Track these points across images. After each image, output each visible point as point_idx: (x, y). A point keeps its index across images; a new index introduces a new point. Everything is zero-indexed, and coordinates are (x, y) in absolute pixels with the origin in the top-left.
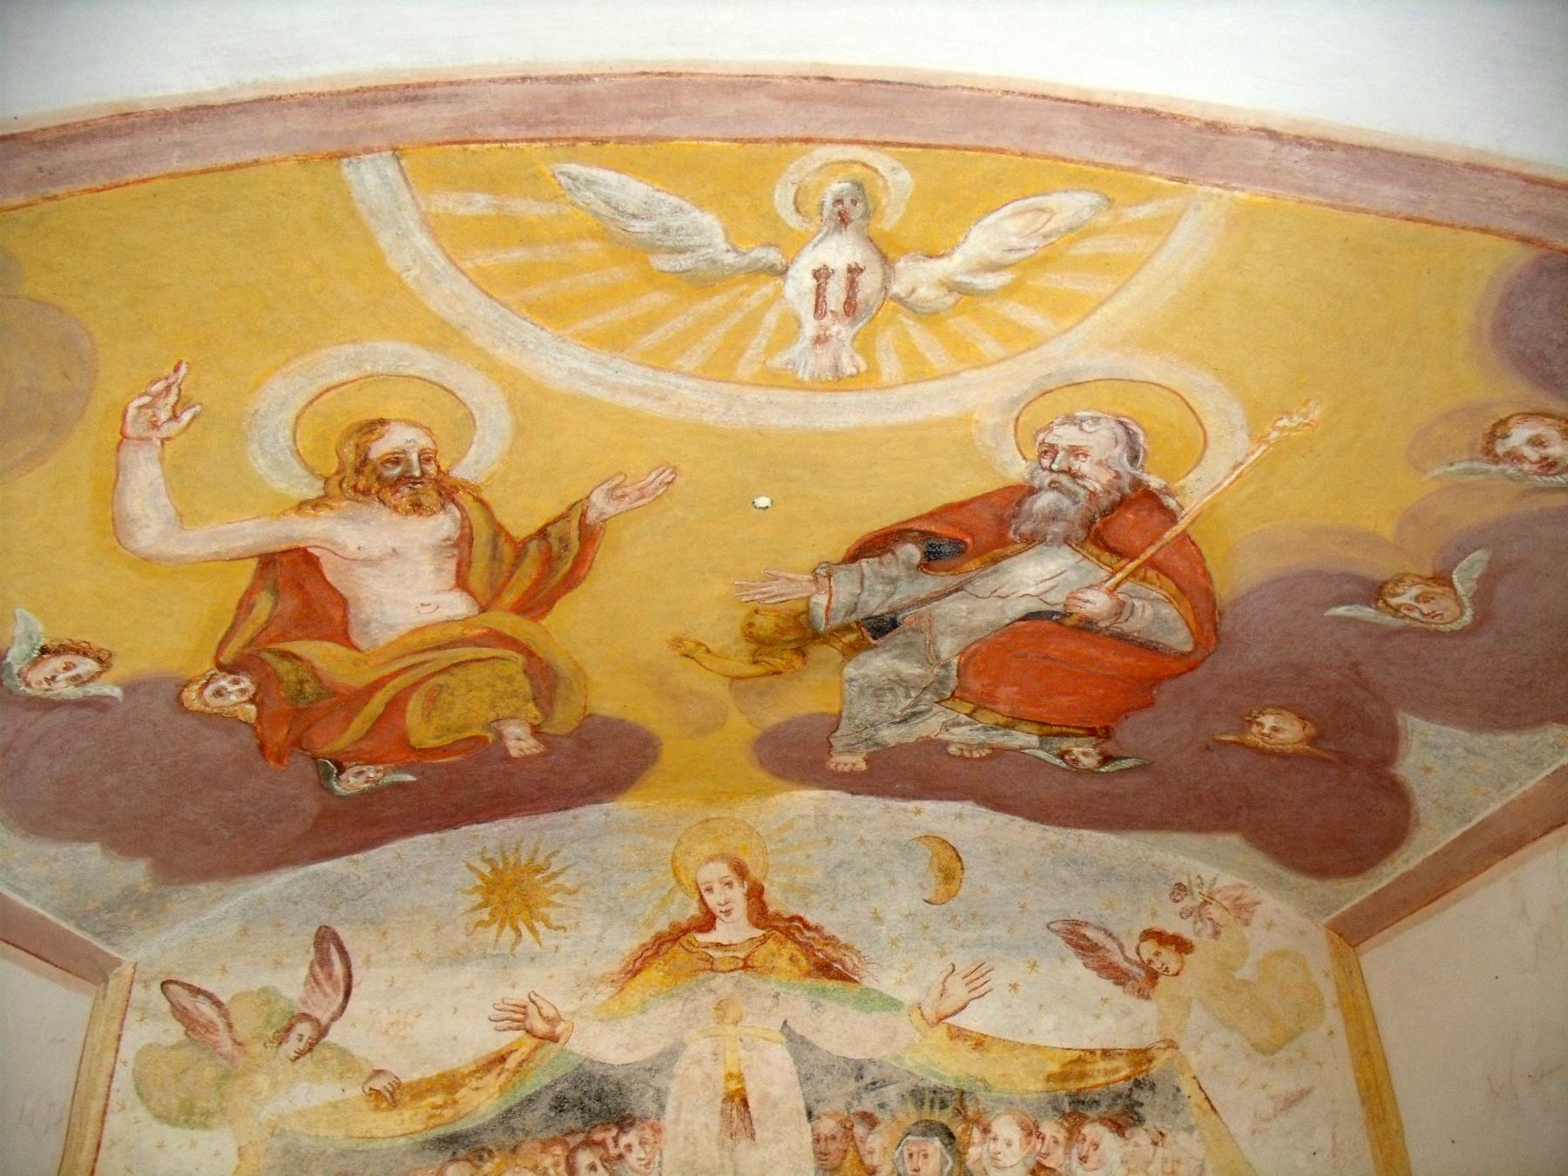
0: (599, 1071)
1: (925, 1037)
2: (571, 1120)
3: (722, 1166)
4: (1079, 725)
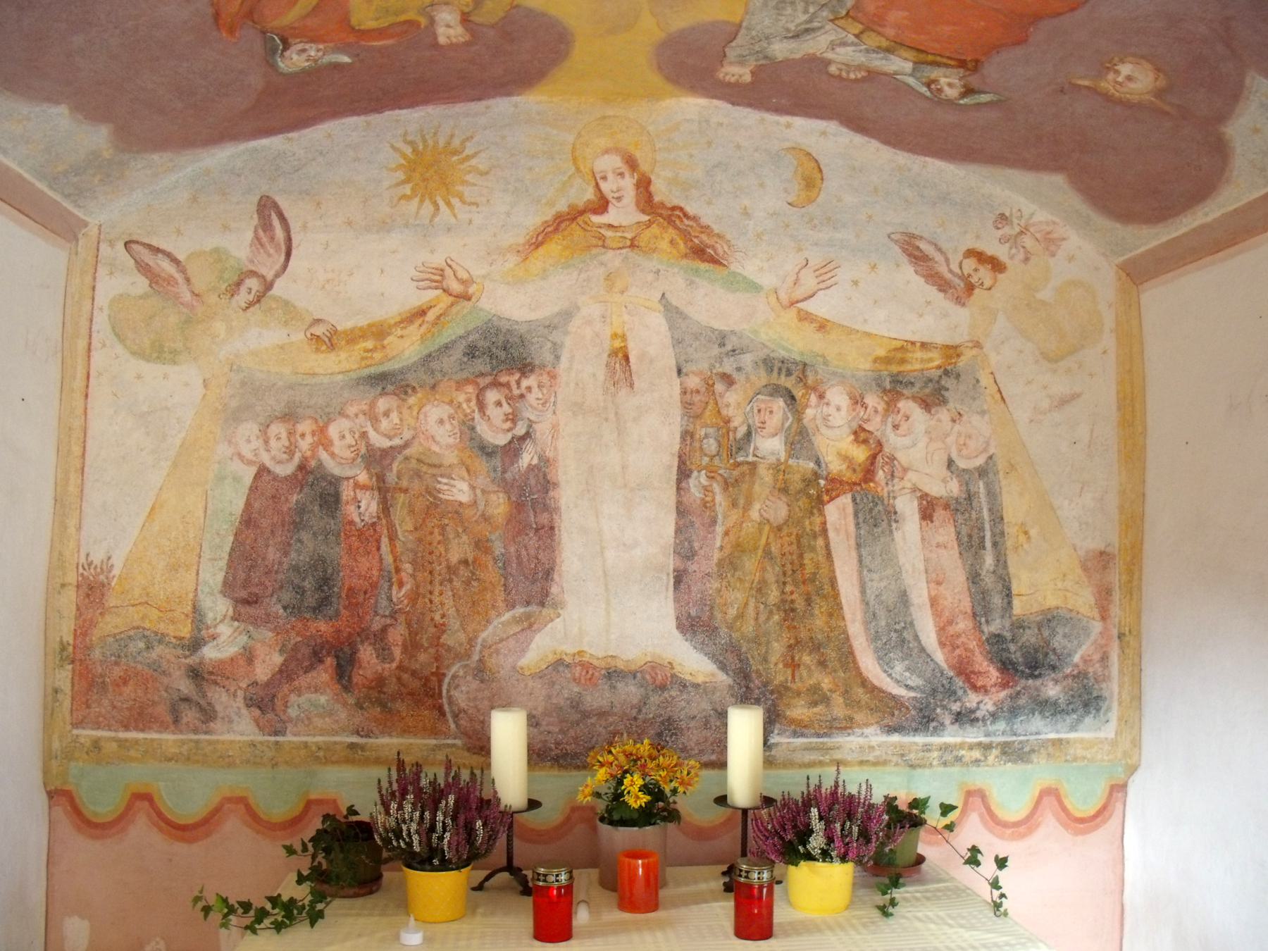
0: (505, 326)
1: (778, 316)
2: (481, 365)
4: (953, 56)
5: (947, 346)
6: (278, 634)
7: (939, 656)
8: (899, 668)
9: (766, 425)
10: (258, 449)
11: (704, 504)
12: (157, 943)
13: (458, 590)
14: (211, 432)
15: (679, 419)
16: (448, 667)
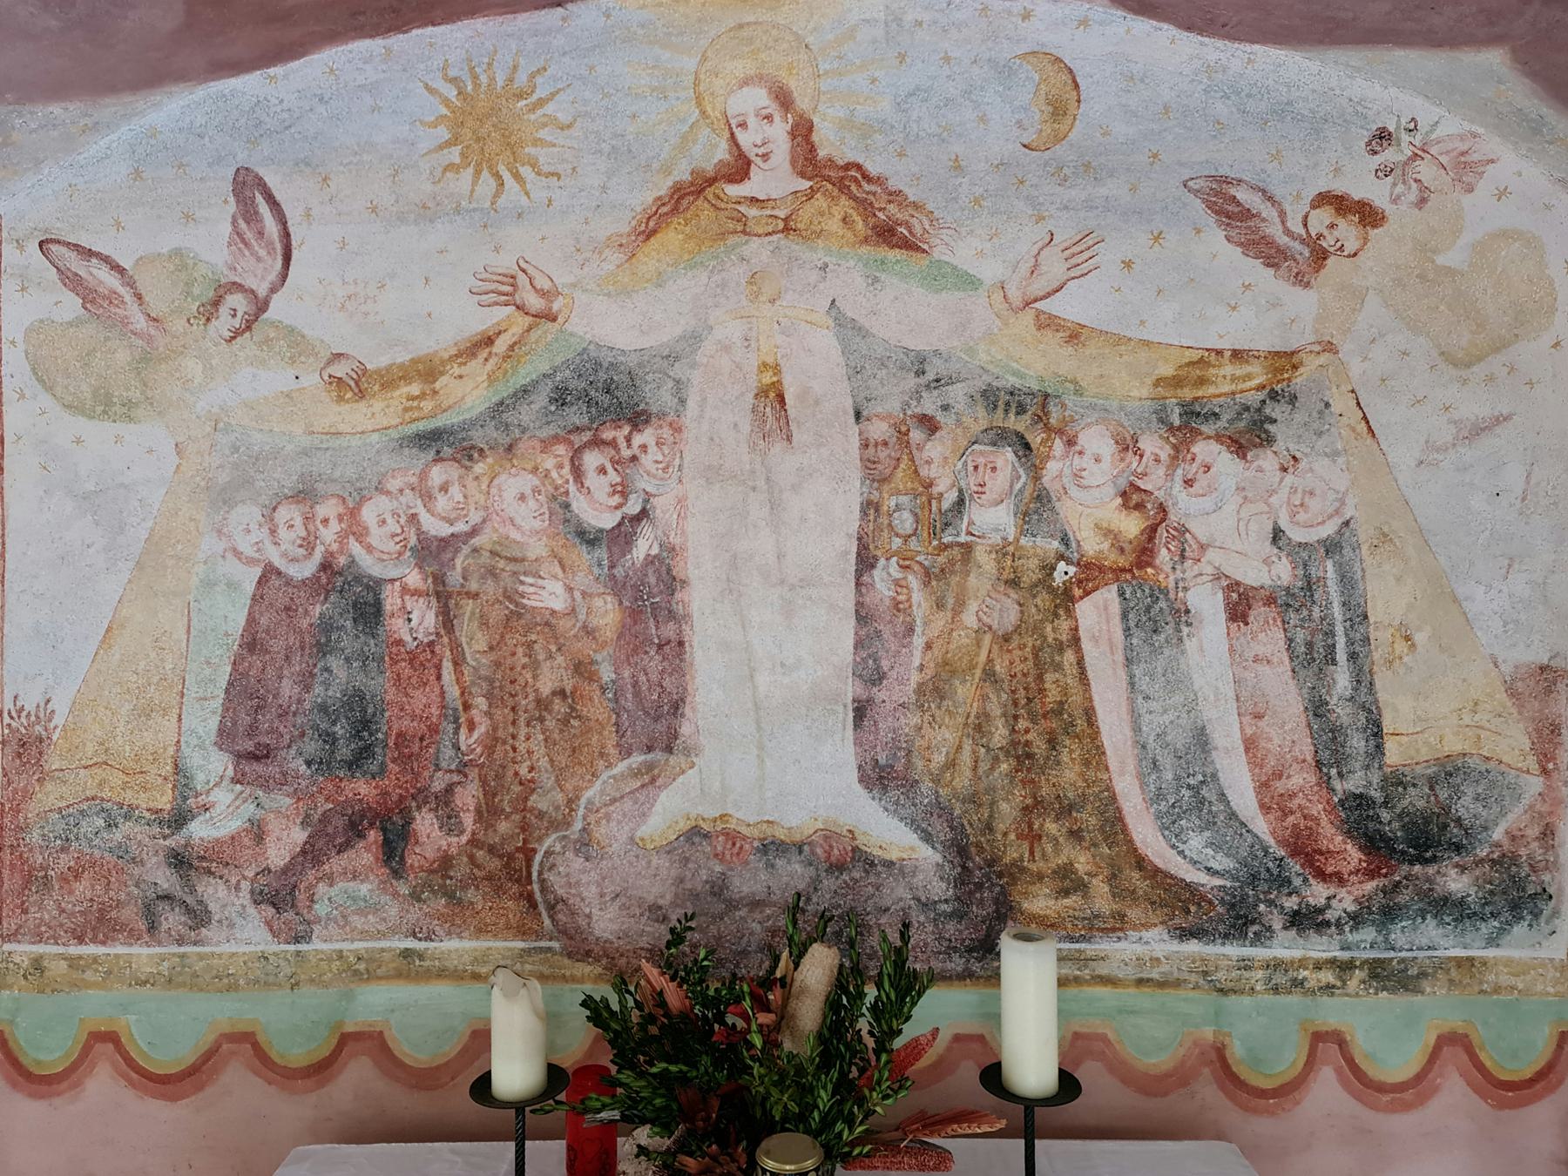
2: (576, 415)
3: (753, 472)
5: (1277, 353)
6: (299, 799)
7: (1261, 826)
9: (986, 489)
10: (261, 541)
11: (896, 605)
13: (552, 732)
14: (191, 520)
15: (858, 484)
16: (540, 840)
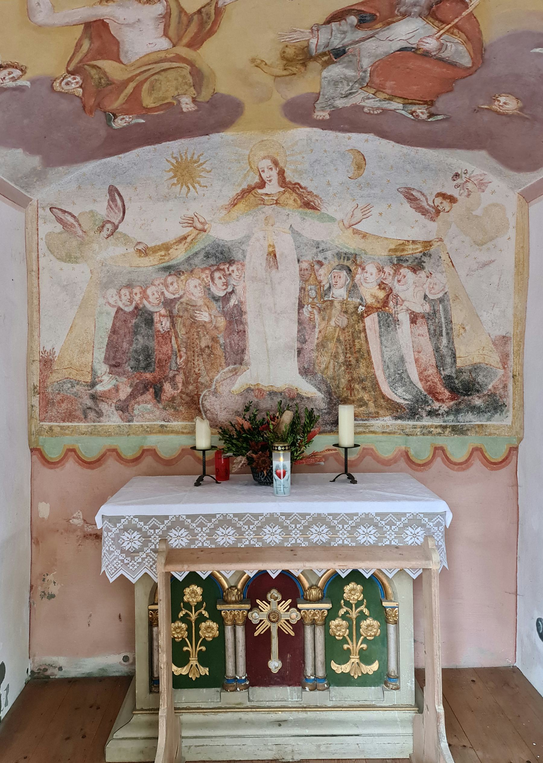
0: (221, 243)
1: (344, 233)
2: (212, 261)
5: (426, 241)
7: (420, 385)
8: (400, 390)
11: (310, 319)
12: (79, 513)
16: (202, 391)
